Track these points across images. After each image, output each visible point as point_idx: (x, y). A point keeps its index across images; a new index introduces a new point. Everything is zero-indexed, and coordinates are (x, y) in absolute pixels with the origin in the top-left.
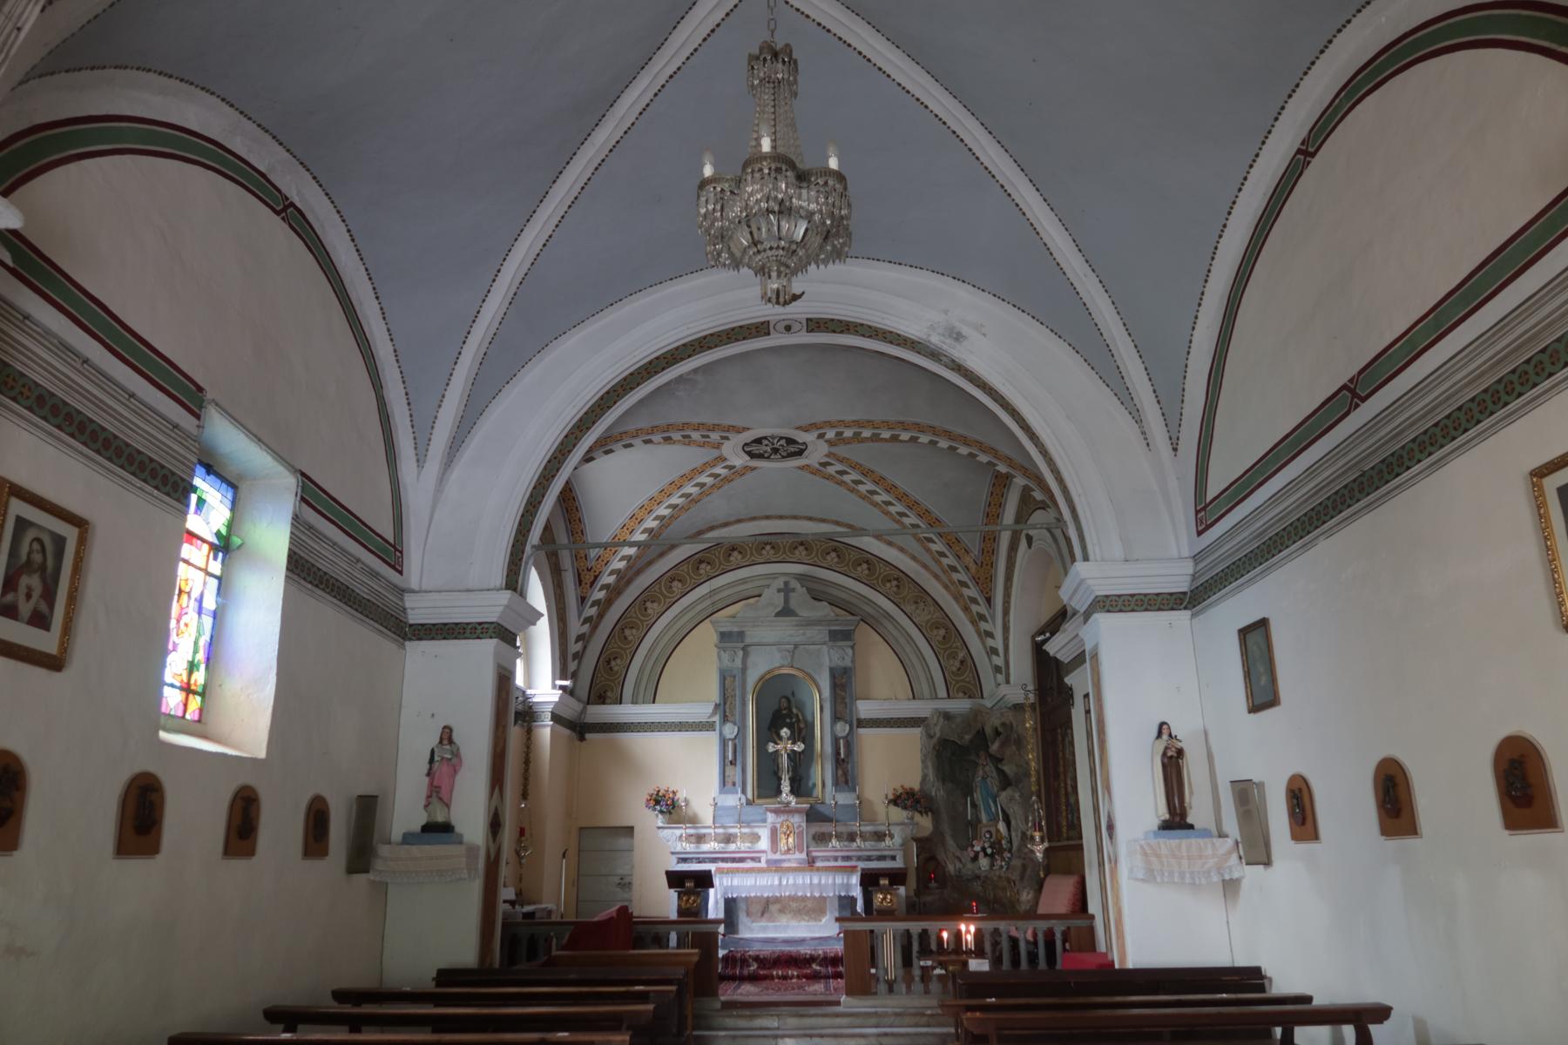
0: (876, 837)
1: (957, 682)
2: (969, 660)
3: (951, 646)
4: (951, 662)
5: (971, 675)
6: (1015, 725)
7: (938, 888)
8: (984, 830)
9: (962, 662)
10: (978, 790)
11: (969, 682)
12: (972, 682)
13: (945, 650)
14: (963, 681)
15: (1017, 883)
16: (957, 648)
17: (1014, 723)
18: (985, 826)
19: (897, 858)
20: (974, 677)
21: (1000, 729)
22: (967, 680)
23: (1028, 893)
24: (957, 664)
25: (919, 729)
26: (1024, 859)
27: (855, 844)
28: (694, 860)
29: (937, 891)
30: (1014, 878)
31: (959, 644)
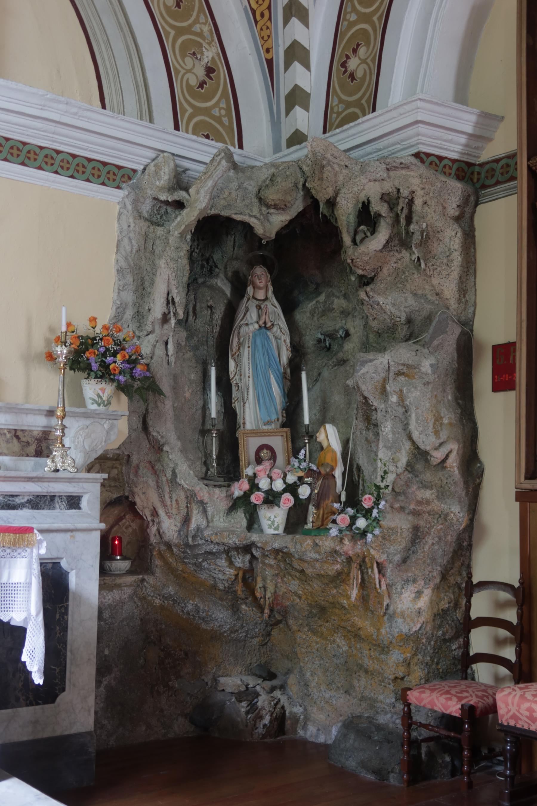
0: (16, 445)
1: (197, 111)
2: (223, 70)
3: (191, 26)
4: (189, 60)
5: (223, 105)
6: (418, 202)
7: (130, 572)
8: (253, 444)
9: (210, 71)
10: (246, 353)
11: (218, 120)
12: (225, 120)
13: (180, 31)
14: (207, 111)
15: (389, 570)
16: (200, 34)
17: (419, 193)
18: (256, 433)
19: (84, 503)
20: (228, 109)
21: (377, 207)
22: (216, 112)
23: (419, 594)
24: (201, 72)
25: (120, 194)
26: (416, 514)
27: (49, 461)
28: (57, 503)
29: (130, 579)
30: (382, 558)
31: (206, 29)
